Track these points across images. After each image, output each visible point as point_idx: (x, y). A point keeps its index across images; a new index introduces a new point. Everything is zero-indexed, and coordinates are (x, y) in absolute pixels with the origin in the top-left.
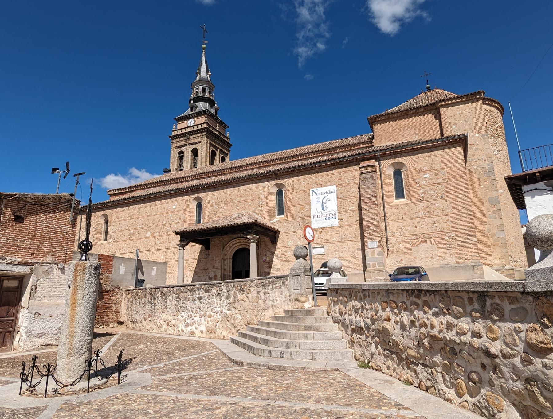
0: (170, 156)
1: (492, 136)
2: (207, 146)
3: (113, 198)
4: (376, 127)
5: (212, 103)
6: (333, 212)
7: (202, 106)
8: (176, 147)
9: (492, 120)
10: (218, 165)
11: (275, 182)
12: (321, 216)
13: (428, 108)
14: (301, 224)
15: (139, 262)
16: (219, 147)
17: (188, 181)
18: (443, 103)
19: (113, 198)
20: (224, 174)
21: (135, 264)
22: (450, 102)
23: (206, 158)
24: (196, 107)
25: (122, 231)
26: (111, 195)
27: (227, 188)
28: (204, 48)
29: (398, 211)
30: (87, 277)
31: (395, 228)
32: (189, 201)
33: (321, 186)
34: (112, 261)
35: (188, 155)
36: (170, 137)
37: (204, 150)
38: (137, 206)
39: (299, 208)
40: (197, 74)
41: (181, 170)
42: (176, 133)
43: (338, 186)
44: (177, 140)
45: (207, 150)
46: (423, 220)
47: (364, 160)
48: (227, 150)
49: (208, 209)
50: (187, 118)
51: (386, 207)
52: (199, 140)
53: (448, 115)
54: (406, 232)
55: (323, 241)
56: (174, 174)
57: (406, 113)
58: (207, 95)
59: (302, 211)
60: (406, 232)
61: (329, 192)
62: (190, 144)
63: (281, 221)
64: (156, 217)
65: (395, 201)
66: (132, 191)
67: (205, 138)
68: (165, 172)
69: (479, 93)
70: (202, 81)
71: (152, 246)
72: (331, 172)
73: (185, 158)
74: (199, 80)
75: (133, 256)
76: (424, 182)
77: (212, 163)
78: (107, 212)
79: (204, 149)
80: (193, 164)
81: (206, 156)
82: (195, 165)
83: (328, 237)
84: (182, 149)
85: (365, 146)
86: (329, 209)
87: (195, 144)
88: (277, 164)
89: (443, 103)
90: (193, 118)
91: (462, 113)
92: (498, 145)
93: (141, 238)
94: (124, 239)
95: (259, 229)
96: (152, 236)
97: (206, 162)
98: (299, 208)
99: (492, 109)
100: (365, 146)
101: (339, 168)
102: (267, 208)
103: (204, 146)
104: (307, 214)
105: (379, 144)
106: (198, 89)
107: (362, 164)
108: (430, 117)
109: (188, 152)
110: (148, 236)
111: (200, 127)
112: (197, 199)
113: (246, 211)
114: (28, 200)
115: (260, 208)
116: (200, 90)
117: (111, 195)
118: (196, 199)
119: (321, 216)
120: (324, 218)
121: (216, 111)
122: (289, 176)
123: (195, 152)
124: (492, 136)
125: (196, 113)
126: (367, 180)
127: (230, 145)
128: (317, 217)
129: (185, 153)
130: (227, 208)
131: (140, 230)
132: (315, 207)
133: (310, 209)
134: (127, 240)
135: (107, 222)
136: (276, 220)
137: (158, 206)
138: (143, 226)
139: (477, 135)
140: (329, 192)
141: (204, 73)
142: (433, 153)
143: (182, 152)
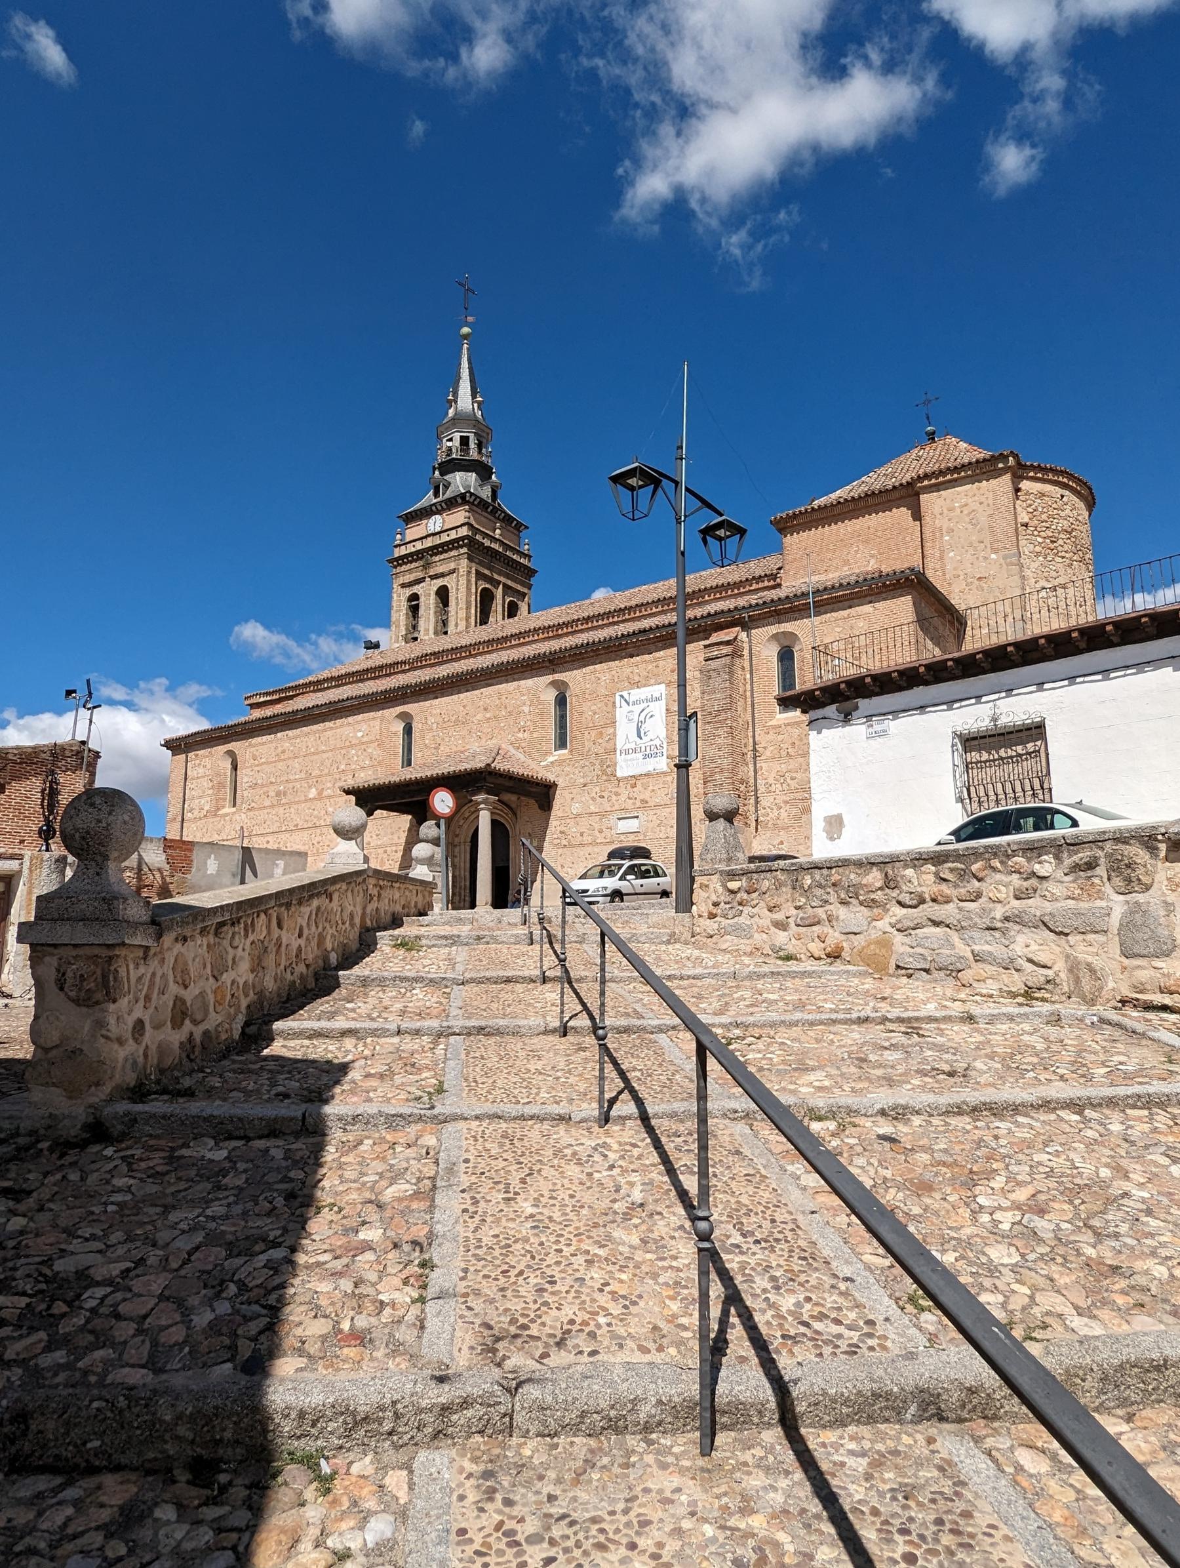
0: (390, 608)
1: (1038, 555)
2: (469, 581)
3: (257, 714)
4: (790, 541)
5: (484, 472)
6: (658, 742)
7: (462, 481)
8: (403, 586)
9: (1044, 517)
10: (499, 625)
11: (550, 678)
12: (634, 751)
13: (897, 494)
14: (597, 767)
15: (247, 852)
16: (502, 579)
17: (403, 672)
18: (926, 483)
19: (257, 714)
20: (475, 656)
21: (238, 856)
22: (941, 479)
23: (468, 608)
24: (446, 487)
25: (262, 786)
26: (252, 706)
27: (459, 692)
28: (466, 337)
29: (780, 737)
30: (45, 871)
31: (773, 774)
32: (387, 721)
33: (637, 685)
34: (191, 851)
35: (429, 602)
36: (390, 561)
37: (463, 589)
38: (290, 733)
39: (593, 733)
40: (449, 403)
41: (415, 639)
42: (403, 551)
44: (404, 568)
45: (469, 589)
47: (720, 627)
48: (523, 584)
49: (422, 738)
52: (452, 566)
53: (937, 510)
54: (793, 784)
55: (638, 804)
57: (851, 506)
58: (473, 454)
60: (793, 784)
61: (652, 699)
62: (432, 577)
63: (560, 762)
64: (325, 756)
65: (779, 716)
66: (291, 698)
67: (464, 562)
69: (1003, 458)
70: (460, 420)
71: (319, 818)
72: (658, 654)
73: (421, 612)
74: (453, 419)
75: (237, 843)
77: (484, 619)
78: (232, 746)
80: (440, 624)
81: (468, 603)
82: (443, 627)
83: (646, 795)
84: (416, 589)
85: (761, 585)
86: (651, 735)
87: (442, 575)
88: (582, 631)
89: (926, 483)
90: (439, 512)
92: (1054, 574)
93: (299, 802)
94: (267, 803)
95: (500, 781)
96: (320, 796)
97: (468, 618)
98: (593, 733)
99: (1047, 488)
100: (761, 585)
102: (535, 735)
103: (463, 581)
104: (610, 746)
105: (791, 584)
107: (715, 637)
108: (902, 514)
109: (427, 593)
110: (311, 796)
111: (453, 535)
112: (231, 753)
113: (494, 741)
114: (10, 756)
115: (520, 735)
116: (456, 443)
117: (252, 706)
119: (634, 751)
120: (640, 756)
122: (577, 664)
123: (443, 595)
124: (1038, 555)
125: (446, 501)
126: (713, 674)
127: (531, 572)
128: (627, 752)
129: (422, 599)
130: (462, 733)
131: (298, 785)
132: (625, 732)
133: (615, 735)
134: (272, 806)
135: (235, 768)
136: (551, 759)
137: (330, 733)
138: (303, 775)
139: (993, 556)
140: (652, 699)
141: (465, 401)
142: (853, 611)
143: (414, 597)
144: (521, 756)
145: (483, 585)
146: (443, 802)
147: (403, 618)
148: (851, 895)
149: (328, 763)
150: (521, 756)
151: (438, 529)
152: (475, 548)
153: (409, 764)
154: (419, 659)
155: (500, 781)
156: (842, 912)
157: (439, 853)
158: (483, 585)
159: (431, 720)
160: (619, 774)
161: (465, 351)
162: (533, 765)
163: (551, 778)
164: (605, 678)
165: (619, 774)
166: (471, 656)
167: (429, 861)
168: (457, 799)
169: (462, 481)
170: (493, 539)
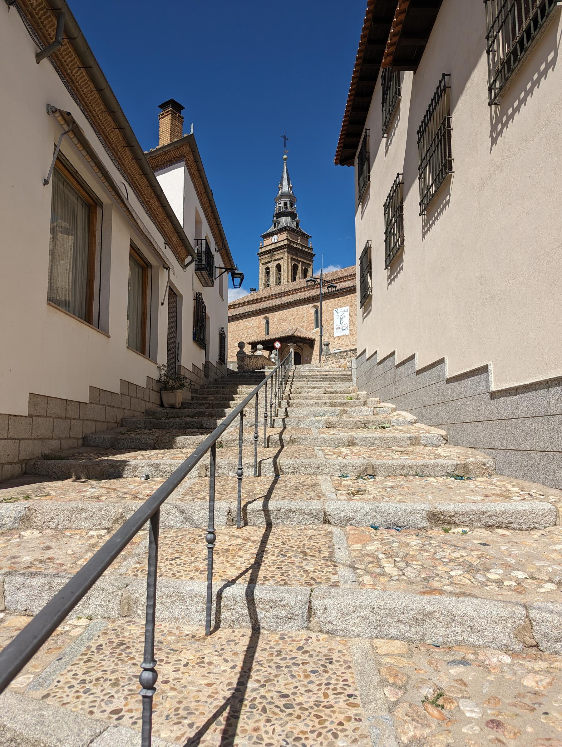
0: (259, 272)
2: (288, 262)
5: (293, 216)
7: (285, 221)
8: (263, 264)
11: (313, 305)
16: (301, 260)
17: (265, 301)
23: (288, 272)
24: (279, 224)
28: (285, 159)
32: (259, 320)
33: (340, 307)
35: (273, 270)
36: (258, 254)
37: (286, 265)
39: (327, 323)
40: (280, 188)
42: (262, 250)
43: (350, 306)
45: (288, 265)
48: (310, 261)
49: (272, 325)
50: (271, 234)
52: (282, 256)
56: (262, 291)
58: (289, 209)
61: (345, 311)
62: (274, 261)
64: (240, 332)
67: (286, 254)
68: (251, 291)
70: (283, 195)
73: (271, 274)
77: (294, 279)
79: (286, 264)
82: (278, 283)
83: (343, 342)
84: (268, 265)
86: (344, 323)
87: (278, 260)
90: (276, 234)
95: (297, 339)
98: (327, 323)
101: (351, 294)
103: (286, 262)
104: (332, 327)
106: (280, 204)
109: (272, 267)
111: (282, 244)
116: (282, 205)
118: (314, 306)
120: (341, 330)
121: (297, 224)
123: (278, 267)
125: (278, 230)
128: (337, 329)
129: (271, 269)
132: (336, 322)
136: (314, 331)
140: (345, 311)
141: (285, 187)
143: (268, 268)
144: (304, 331)
145: (294, 263)
146: (278, 345)
147: (263, 277)
148: (342, 357)
149: (241, 334)
150: (304, 331)
151: (276, 241)
152: (290, 249)
153: (268, 334)
154: (270, 296)
155: (297, 339)
156: (341, 360)
157: (277, 358)
158: (294, 263)
159: (275, 319)
160: (335, 336)
161: (285, 166)
162: (308, 334)
163: (314, 338)
164: (330, 304)
165: (335, 336)
166: (288, 295)
167: (274, 358)
168: (281, 345)
169: (285, 221)
170: (297, 244)
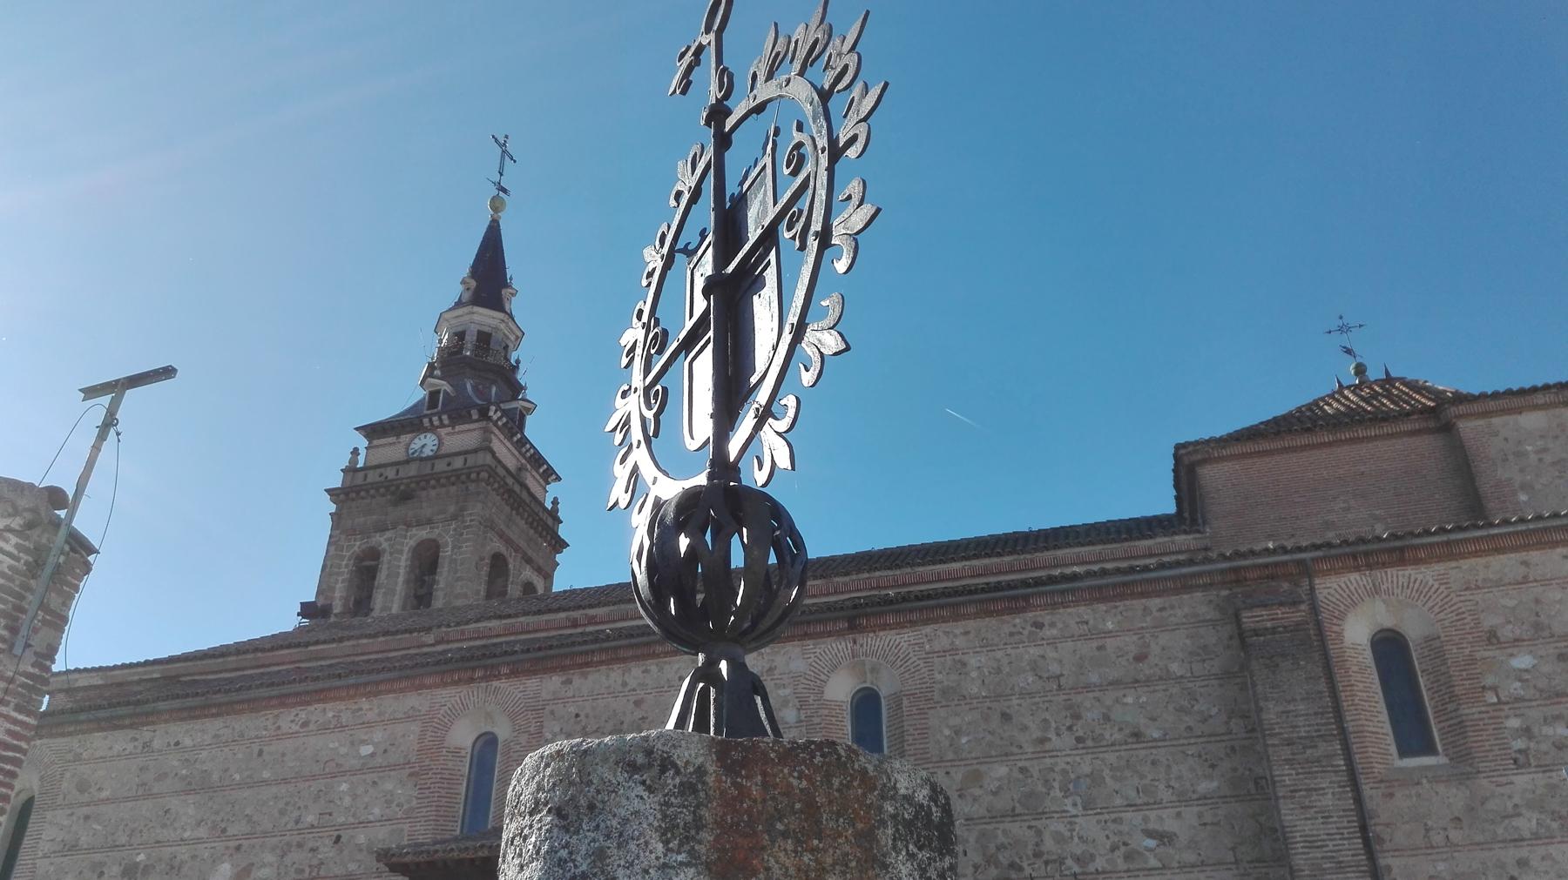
46: (1541, 851)
51: (1367, 790)
59: (977, 792)
73: (382, 577)
76: (1515, 687)
91: (1545, 450)
129: (386, 558)
138: (202, 832)
143: (374, 554)
